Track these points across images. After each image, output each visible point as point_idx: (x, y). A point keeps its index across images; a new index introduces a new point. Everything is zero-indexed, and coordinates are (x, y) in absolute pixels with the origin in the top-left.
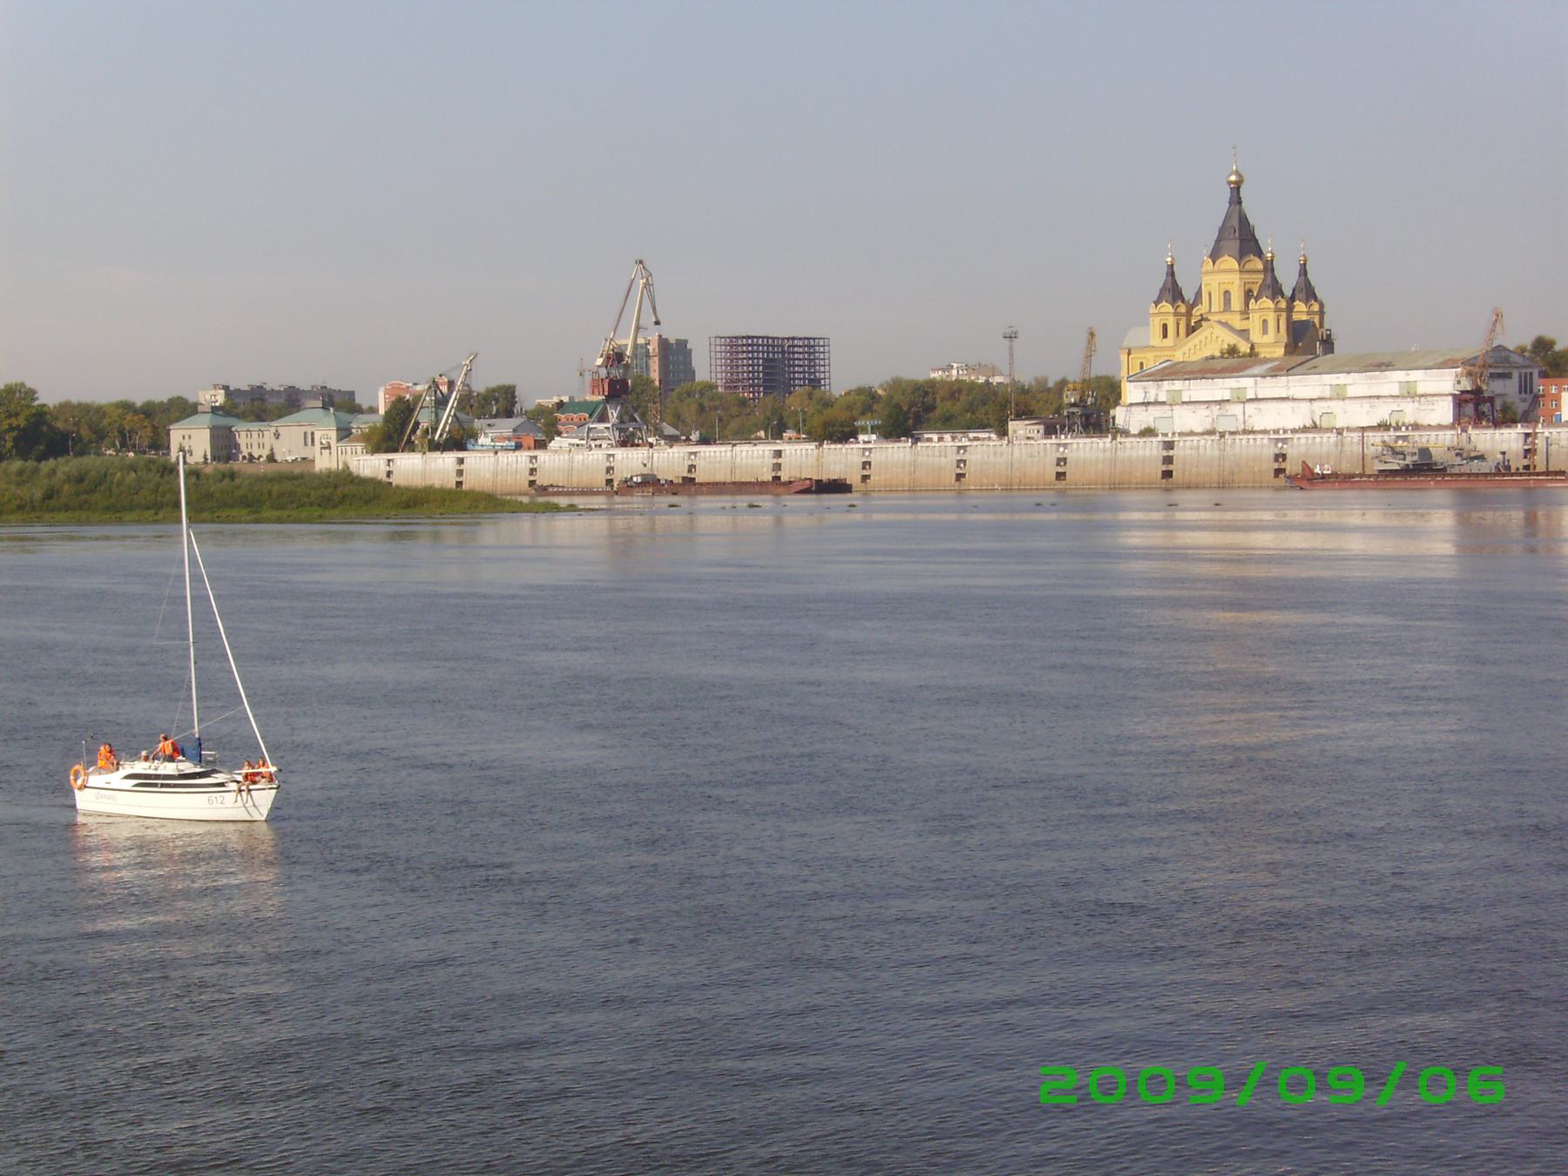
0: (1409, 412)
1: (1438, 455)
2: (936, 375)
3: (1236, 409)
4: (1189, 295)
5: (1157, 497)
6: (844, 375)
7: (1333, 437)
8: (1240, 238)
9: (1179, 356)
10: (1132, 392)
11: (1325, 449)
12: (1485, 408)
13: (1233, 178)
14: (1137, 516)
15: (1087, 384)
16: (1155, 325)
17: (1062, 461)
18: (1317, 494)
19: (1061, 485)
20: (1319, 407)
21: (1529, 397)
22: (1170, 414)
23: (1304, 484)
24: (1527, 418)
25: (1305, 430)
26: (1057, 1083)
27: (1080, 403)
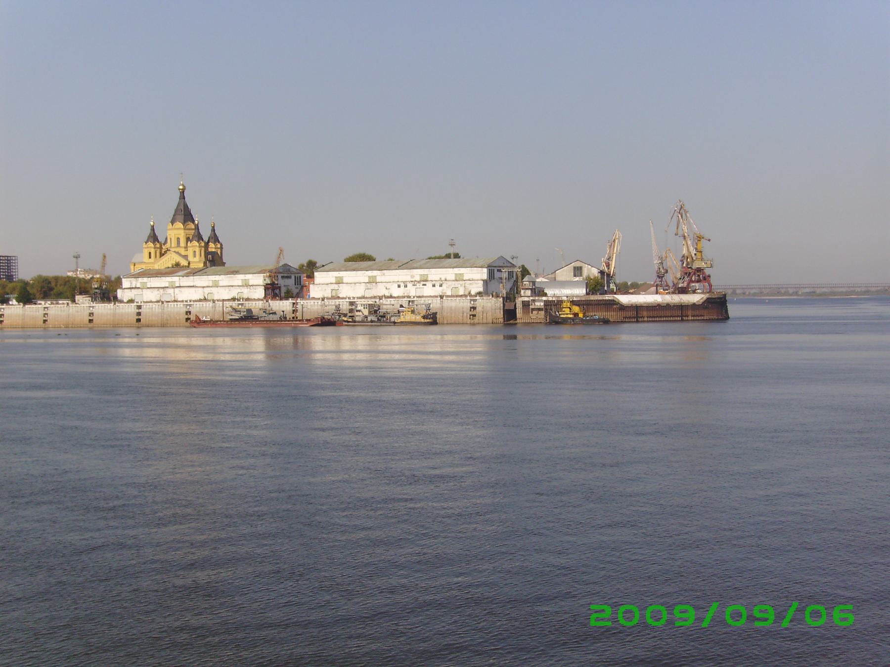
0: (246, 293)
1: (255, 312)
2: (70, 274)
3: (171, 291)
4: (161, 239)
5: (134, 331)
6: (26, 272)
7: (211, 304)
8: (185, 214)
9: (156, 267)
10: (126, 283)
11: (316, 307)
12: (277, 291)
13: (181, 187)
14: (127, 340)
15: (101, 281)
16: (146, 253)
17: (91, 314)
18: (201, 330)
19: (90, 325)
20: (207, 290)
21: (299, 287)
22: (142, 293)
23: (196, 325)
24: (298, 295)
25: (200, 300)
26: (600, 616)
27: (100, 288)
